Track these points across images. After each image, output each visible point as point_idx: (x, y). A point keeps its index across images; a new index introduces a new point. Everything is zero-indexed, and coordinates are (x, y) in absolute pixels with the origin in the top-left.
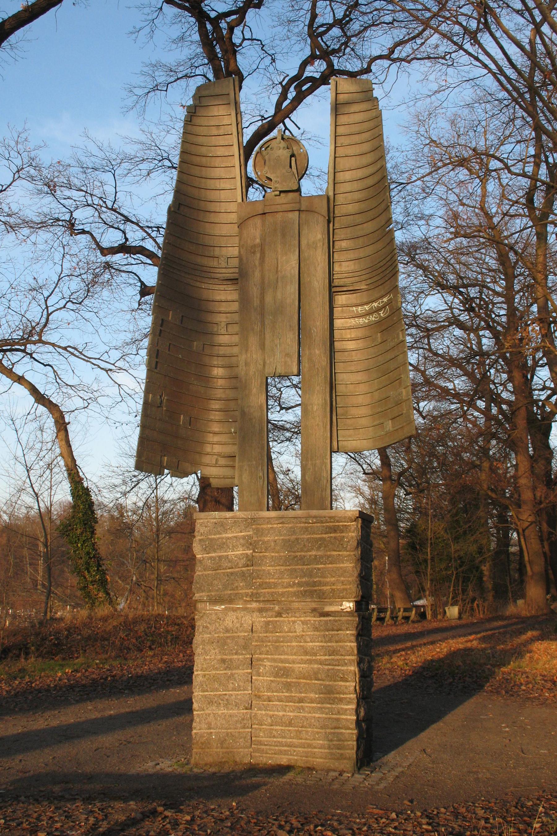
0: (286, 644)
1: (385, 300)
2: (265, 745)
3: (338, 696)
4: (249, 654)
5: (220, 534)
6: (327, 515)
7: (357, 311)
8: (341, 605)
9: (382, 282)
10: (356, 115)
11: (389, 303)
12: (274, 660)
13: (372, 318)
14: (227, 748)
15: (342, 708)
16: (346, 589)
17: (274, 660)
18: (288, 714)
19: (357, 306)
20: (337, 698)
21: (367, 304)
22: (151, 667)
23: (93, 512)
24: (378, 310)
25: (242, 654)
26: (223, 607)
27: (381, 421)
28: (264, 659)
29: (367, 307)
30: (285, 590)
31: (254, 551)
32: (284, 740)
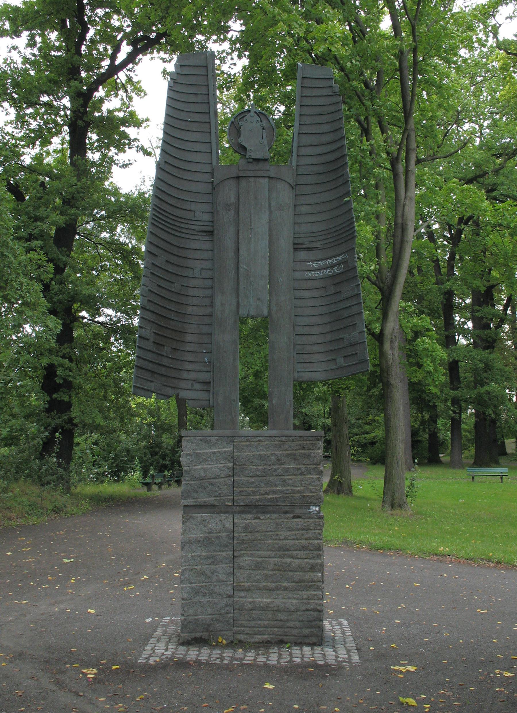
1: (340, 258)
2: (245, 627)
3: (286, 553)
4: (231, 551)
5: (206, 449)
6: (297, 435)
7: (313, 266)
8: (309, 509)
9: (336, 243)
10: (323, 98)
11: (345, 262)
13: (327, 272)
16: (314, 496)
19: (312, 261)
21: (322, 260)
22: (235, 615)
24: (332, 266)
25: (226, 551)
27: (334, 357)
29: (322, 263)
30: (262, 497)
31: (235, 464)
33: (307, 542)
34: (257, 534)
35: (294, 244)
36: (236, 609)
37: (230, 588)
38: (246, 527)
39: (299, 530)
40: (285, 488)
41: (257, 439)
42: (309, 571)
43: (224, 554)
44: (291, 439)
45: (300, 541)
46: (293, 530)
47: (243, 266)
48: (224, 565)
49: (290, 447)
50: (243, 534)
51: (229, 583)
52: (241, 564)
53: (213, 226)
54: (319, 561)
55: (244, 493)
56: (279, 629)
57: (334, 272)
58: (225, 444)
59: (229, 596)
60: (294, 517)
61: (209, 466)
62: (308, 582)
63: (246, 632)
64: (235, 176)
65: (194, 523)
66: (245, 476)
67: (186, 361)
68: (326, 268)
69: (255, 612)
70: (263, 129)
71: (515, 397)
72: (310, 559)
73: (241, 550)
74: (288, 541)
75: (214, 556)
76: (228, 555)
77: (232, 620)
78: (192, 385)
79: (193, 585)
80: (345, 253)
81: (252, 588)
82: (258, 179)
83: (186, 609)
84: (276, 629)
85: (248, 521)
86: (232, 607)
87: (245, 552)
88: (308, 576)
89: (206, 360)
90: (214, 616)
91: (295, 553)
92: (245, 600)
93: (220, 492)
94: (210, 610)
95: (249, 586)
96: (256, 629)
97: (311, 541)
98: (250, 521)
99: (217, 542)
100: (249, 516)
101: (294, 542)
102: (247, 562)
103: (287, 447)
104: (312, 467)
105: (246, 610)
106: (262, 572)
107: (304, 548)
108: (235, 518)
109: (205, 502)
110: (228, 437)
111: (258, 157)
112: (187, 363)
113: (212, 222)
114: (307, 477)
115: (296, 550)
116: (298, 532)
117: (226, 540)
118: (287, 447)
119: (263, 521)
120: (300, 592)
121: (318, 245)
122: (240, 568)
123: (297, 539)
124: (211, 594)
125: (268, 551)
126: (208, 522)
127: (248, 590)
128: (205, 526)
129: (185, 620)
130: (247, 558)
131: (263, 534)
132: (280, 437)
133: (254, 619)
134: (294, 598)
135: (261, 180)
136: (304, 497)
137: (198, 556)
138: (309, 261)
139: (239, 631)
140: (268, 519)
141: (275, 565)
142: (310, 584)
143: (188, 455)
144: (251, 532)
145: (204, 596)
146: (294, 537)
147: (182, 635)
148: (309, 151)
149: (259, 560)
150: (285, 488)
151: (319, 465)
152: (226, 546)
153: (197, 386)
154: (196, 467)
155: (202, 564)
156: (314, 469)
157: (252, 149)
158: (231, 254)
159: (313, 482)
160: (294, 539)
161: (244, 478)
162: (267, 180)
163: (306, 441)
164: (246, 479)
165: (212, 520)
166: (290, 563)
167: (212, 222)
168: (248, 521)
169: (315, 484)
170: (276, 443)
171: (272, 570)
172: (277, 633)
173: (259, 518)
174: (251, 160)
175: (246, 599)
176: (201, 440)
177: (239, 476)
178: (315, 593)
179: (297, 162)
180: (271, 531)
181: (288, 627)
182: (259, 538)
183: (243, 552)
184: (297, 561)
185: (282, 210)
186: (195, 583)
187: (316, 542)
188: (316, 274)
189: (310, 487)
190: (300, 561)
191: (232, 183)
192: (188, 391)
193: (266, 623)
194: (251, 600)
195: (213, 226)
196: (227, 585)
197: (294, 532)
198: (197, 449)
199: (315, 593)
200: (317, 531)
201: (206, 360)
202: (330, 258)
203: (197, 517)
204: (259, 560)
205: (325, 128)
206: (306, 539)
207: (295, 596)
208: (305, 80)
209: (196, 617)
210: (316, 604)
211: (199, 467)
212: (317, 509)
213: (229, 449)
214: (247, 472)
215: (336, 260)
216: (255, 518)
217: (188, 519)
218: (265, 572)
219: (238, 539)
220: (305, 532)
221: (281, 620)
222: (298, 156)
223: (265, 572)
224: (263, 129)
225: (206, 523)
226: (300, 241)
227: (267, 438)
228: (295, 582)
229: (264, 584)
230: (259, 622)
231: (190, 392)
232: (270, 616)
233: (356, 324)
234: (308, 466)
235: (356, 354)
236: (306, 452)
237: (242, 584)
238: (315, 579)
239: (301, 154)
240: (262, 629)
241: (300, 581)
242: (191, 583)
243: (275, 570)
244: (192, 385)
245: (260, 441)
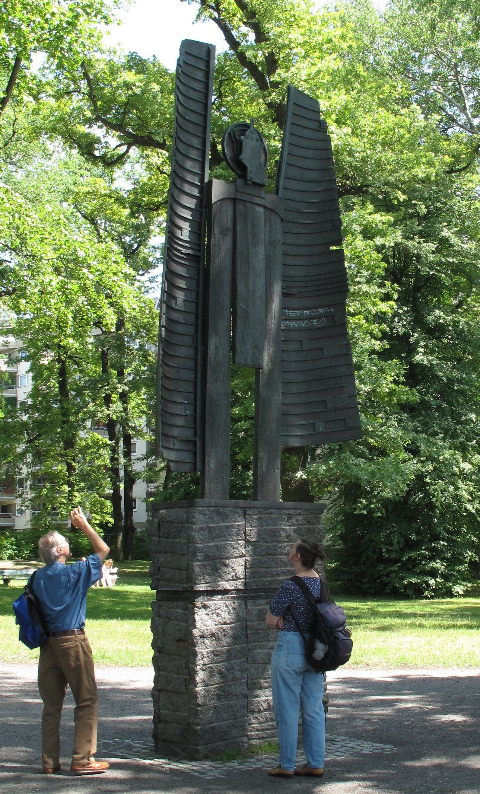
1: (321, 311)
5: (219, 523)
13: (304, 324)
21: (298, 309)
24: (310, 318)
25: (239, 644)
29: (298, 313)
41: (269, 511)
47: (241, 306)
48: (238, 661)
51: (243, 681)
55: (256, 575)
57: (312, 325)
61: (222, 543)
63: (260, 736)
68: (303, 320)
76: (243, 647)
80: (330, 306)
94: (225, 715)
98: (263, 607)
100: (263, 601)
108: (249, 604)
118: (294, 521)
135: (257, 208)
143: (202, 529)
154: (209, 544)
158: (226, 289)
183: (254, 644)
198: (210, 523)
202: (307, 309)
209: (212, 725)
211: (212, 544)
215: (316, 312)
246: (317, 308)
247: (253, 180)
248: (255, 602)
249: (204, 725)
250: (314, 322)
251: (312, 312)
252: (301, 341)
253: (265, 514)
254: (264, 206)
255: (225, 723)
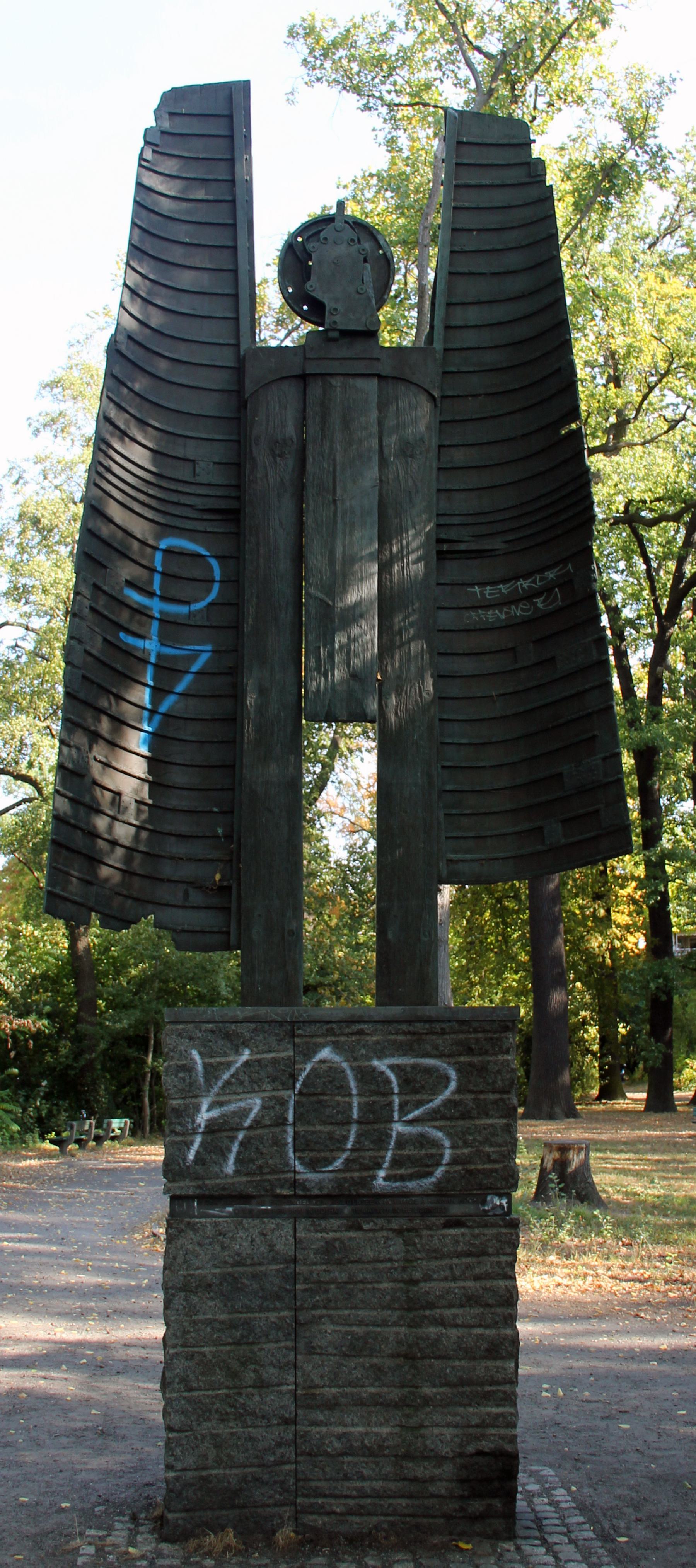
0: (369, 1286)
1: (551, 575)
3: (428, 1312)
4: (290, 1309)
8: (484, 1202)
11: (566, 583)
12: (346, 1322)
13: (517, 611)
14: (244, 1507)
15: (488, 1414)
16: (496, 1171)
17: (346, 1322)
18: (375, 1430)
19: (482, 584)
20: (425, 1317)
21: (504, 581)
23: (484, 115)
24: (530, 596)
25: (275, 1309)
26: (230, 1209)
28: (321, 1317)
29: (503, 588)
32: (366, 1484)
33: (478, 1284)
34: (354, 1267)
35: (439, 541)
36: (303, 1453)
37: (288, 1401)
38: (328, 1249)
39: (459, 1255)
40: (423, 1152)
42: (485, 1358)
43: (273, 1316)
44: (438, 1026)
45: (461, 1284)
46: (443, 1257)
49: (436, 1047)
50: (319, 1268)
51: (284, 1388)
52: (316, 1342)
53: (238, 498)
54: (509, 1332)
56: (409, 1501)
57: (537, 609)
58: (272, 1040)
59: (286, 1422)
60: (448, 1225)
62: (482, 1384)
64: (298, 372)
65: (196, 1239)
66: (324, 1123)
67: (170, 834)
68: (515, 602)
69: (350, 1459)
70: (365, 261)
71: (626, 768)
72: (487, 1327)
73: (315, 1307)
74: (433, 1284)
75: (247, 1322)
77: (292, 1481)
78: (186, 895)
79: (195, 1394)
80: (564, 561)
81: (343, 1400)
82: (351, 381)
83: (178, 1451)
84: (403, 1502)
85: (331, 1235)
86: (292, 1448)
87: (324, 1312)
88: (483, 1368)
89: (220, 831)
90: (249, 1470)
91: (448, 1313)
92: (324, 1429)
93: (260, 1162)
95: (335, 1397)
96: (351, 1502)
97: (488, 1284)
98: (338, 1235)
99: (255, 1286)
100: (335, 1223)
101: (447, 1285)
102: (330, 1337)
103: (428, 1047)
104: (492, 1097)
105: (327, 1454)
106: (367, 1362)
107: (470, 1300)
108: (300, 1227)
109: (224, 1189)
110: (281, 1024)
111: (352, 327)
112: (173, 839)
113: (238, 487)
114: (477, 1122)
115: (450, 1306)
116: (456, 1261)
117: (277, 1281)
118: (428, 1047)
119: (371, 1234)
120: (461, 1410)
121: (497, 544)
122: (311, 1350)
123: (455, 1279)
124: (239, 1417)
125: (383, 1308)
126: (233, 1239)
127: (332, 1405)
128: (223, 1248)
129: (177, 1479)
130: (330, 1328)
131: (369, 1266)
132: (410, 1022)
133: (346, 1478)
134: (448, 1425)
135: (360, 383)
136: (470, 1172)
137: (209, 1322)
138: (472, 585)
139: (312, 1505)
140: (382, 1229)
141: (399, 1342)
142: (488, 1388)
144: (339, 1263)
145: (223, 1420)
146: (447, 1273)
147: (170, 1516)
148: (473, 315)
149: (359, 1330)
150: (423, 1152)
151: (508, 1092)
152: (279, 1298)
153: (196, 897)
155: (217, 1343)
156: (495, 1102)
157: (339, 307)
158: (284, 565)
159: (494, 1135)
160: (446, 1279)
161: (319, 1128)
162: (373, 385)
163: (476, 1031)
164: (327, 1128)
165: (241, 1234)
166: (438, 1340)
167: (238, 487)
168: (331, 1235)
169: (500, 1140)
170: (400, 1038)
171: (392, 1356)
172: (406, 1511)
173: (360, 1228)
174: (335, 334)
175: (329, 1430)
176: (213, 1032)
177: (309, 1123)
178: (500, 1410)
179: (446, 340)
180: (390, 1260)
181: (432, 1496)
182: (360, 1276)
183: (318, 1312)
184: (454, 1333)
185: (412, 456)
186: (199, 1389)
187: (502, 1283)
188: (491, 616)
189: (487, 1149)
190: (461, 1331)
191: (290, 391)
192: (174, 910)
193: (378, 1485)
194: (340, 1430)
195: (238, 498)
196: (280, 1392)
197: (446, 1262)
199: (500, 1410)
200: (503, 1258)
201: (220, 831)
202: (525, 577)
203: (204, 1226)
204: (359, 1330)
205: (513, 260)
206: (477, 1278)
207: (450, 1419)
208: (465, 149)
210: (502, 1437)
212: (504, 1202)
213: (283, 1055)
214: (328, 1111)
216: (349, 1228)
217: (181, 1231)
218: (375, 1360)
219: (306, 1280)
220: (474, 1260)
221: (415, 1480)
222: (447, 328)
223: (375, 1360)
224: (365, 261)
225: (227, 1241)
226: (453, 534)
227: (379, 1026)
228: (448, 1384)
229: (372, 1390)
230: (358, 1484)
231: (180, 913)
232: (388, 1469)
233: (594, 737)
234: (482, 1097)
235: (597, 812)
236: (476, 1060)
237: (318, 1391)
238: (500, 1377)
239: (453, 324)
240: (369, 1501)
241: (462, 1382)
242: (191, 1390)
243: (399, 1356)
244: (186, 895)
245: (361, 1032)
246: (542, 570)
247: (341, 327)
248: (313, 1224)
249: (184, 1470)
250: (539, 602)
251: (534, 582)
252: (513, 649)
253: (347, 1035)
254: (379, 376)
255: (234, 1471)
